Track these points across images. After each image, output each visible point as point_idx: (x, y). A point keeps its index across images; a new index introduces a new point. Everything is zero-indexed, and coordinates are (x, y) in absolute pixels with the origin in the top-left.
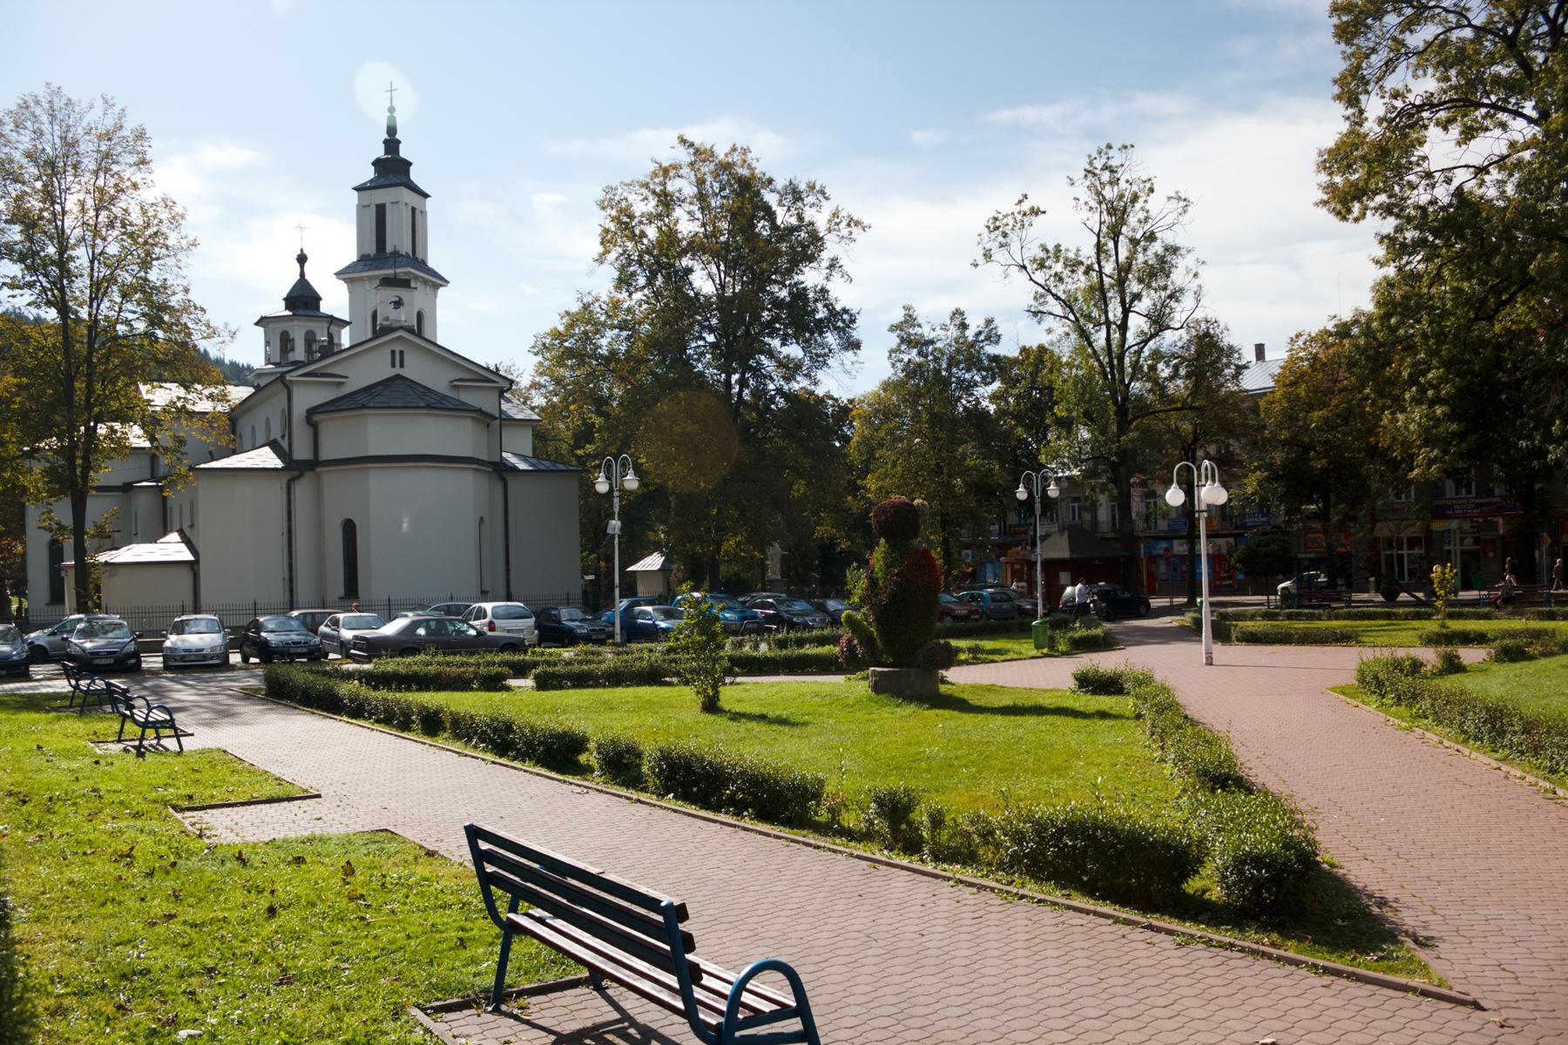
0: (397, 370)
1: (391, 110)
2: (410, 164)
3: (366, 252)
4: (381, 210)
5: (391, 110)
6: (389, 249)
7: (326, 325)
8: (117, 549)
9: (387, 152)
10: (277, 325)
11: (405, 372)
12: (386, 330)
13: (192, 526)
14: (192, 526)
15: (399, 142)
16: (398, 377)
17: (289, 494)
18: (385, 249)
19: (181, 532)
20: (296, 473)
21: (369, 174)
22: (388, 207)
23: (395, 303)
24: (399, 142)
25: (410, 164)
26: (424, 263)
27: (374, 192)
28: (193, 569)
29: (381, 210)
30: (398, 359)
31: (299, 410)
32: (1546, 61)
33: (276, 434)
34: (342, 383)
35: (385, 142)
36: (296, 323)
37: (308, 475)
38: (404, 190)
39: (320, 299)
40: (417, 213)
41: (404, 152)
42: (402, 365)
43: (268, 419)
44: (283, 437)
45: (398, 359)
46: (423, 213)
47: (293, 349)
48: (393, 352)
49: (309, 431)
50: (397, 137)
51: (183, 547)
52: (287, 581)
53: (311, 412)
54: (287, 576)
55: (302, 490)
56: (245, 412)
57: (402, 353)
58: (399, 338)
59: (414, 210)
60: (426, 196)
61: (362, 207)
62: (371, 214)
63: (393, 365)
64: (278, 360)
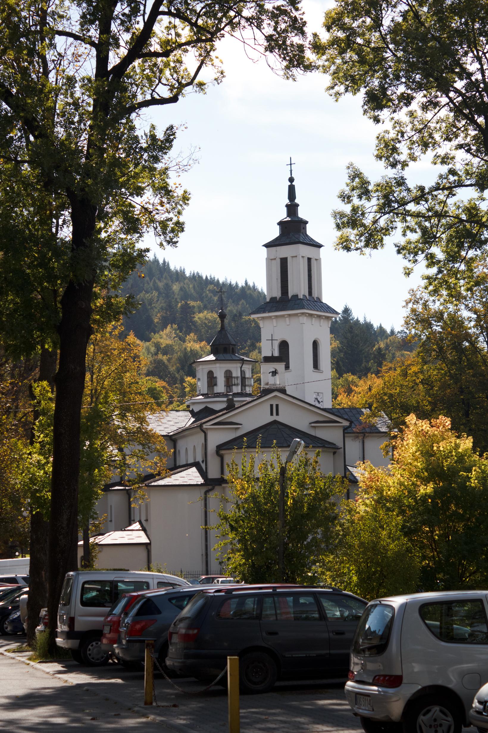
0: (275, 418)
1: (291, 180)
2: (306, 222)
3: (274, 296)
4: (284, 262)
5: (291, 180)
6: (290, 295)
7: (239, 365)
8: (103, 534)
9: (288, 215)
10: (204, 367)
11: (280, 419)
12: (267, 392)
13: (147, 520)
14: (147, 520)
15: (297, 205)
16: (275, 422)
17: (206, 500)
18: (287, 293)
19: (141, 523)
20: (210, 487)
21: (275, 233)
22: (289, 261)
23: (273, 372)
24: (297, 205)
25: (306, 222)
26: (319, 300)
27: (279, 248)
28: (147, 548)
29: (284, 262)
30: (274, 410)
31: (212, 446)
32: (293, 545)
33: (199, 459)
34: (239, 428)
35: (287, 206)
36: (218, 365)
37: (217, 488)
38: (301, 246)
39: (295, 198)
40: (313, 262)
41: (302, 214)
42: (277, 414)
43: (194, 446)
44: (203, 462)
45: (274, 410)
46: (318, 260)
47: (216, 385)
48: (272, 406)
49: (217, 460)
50: (297, 201)
51: (142, 533)
52: (204, 557)
53: (220, 448)
54: (204, 553)
55: (213, 496)
56: (184, 437)
57: (277, 406)
58: (275, 396)
59: (309, 260)
60: (319, 246)
61: (270, 260)
62: (277, 265)
63: (272, 414)
64: (205, 392)
